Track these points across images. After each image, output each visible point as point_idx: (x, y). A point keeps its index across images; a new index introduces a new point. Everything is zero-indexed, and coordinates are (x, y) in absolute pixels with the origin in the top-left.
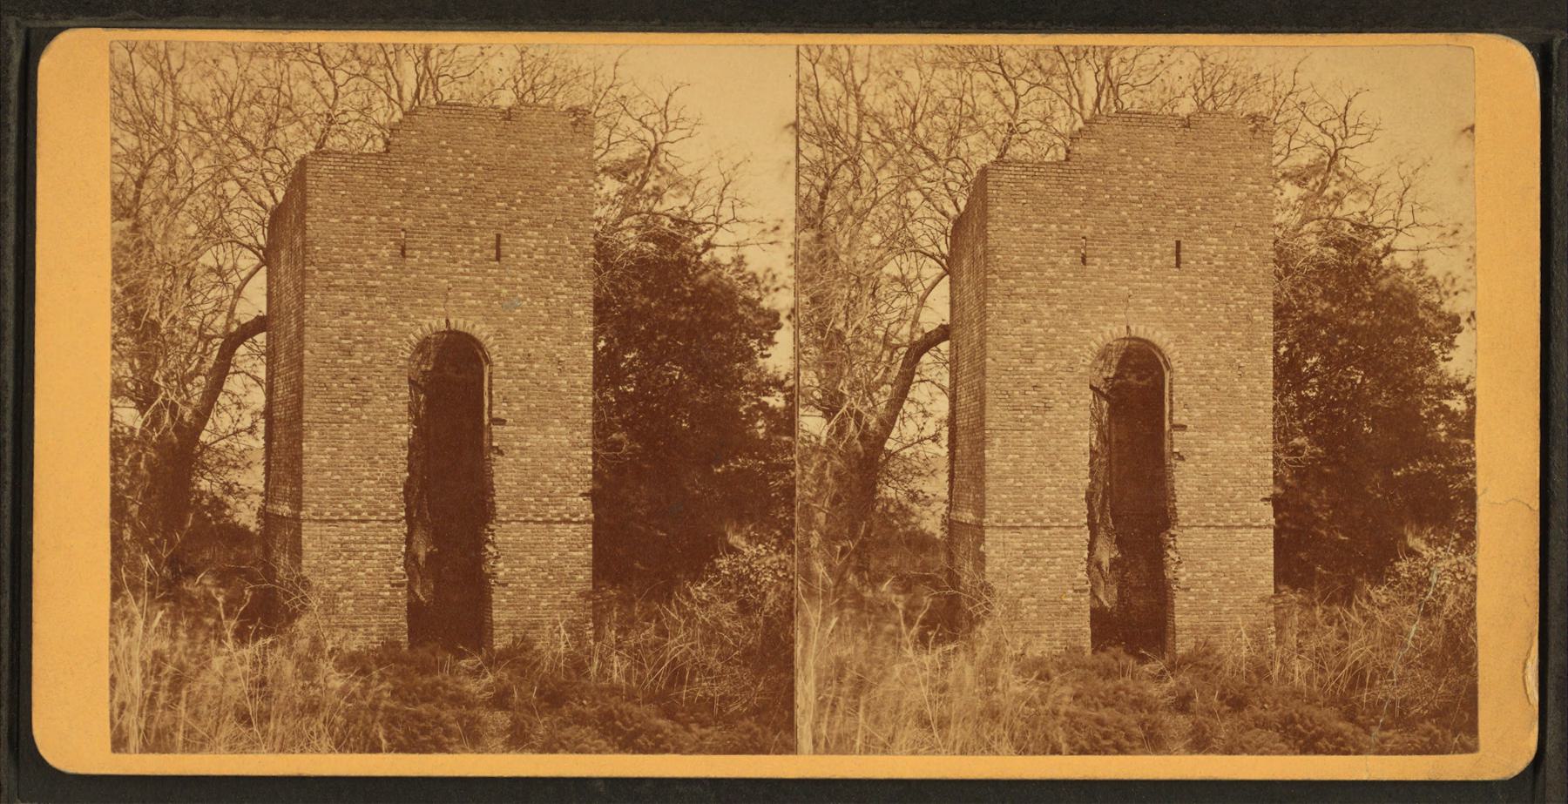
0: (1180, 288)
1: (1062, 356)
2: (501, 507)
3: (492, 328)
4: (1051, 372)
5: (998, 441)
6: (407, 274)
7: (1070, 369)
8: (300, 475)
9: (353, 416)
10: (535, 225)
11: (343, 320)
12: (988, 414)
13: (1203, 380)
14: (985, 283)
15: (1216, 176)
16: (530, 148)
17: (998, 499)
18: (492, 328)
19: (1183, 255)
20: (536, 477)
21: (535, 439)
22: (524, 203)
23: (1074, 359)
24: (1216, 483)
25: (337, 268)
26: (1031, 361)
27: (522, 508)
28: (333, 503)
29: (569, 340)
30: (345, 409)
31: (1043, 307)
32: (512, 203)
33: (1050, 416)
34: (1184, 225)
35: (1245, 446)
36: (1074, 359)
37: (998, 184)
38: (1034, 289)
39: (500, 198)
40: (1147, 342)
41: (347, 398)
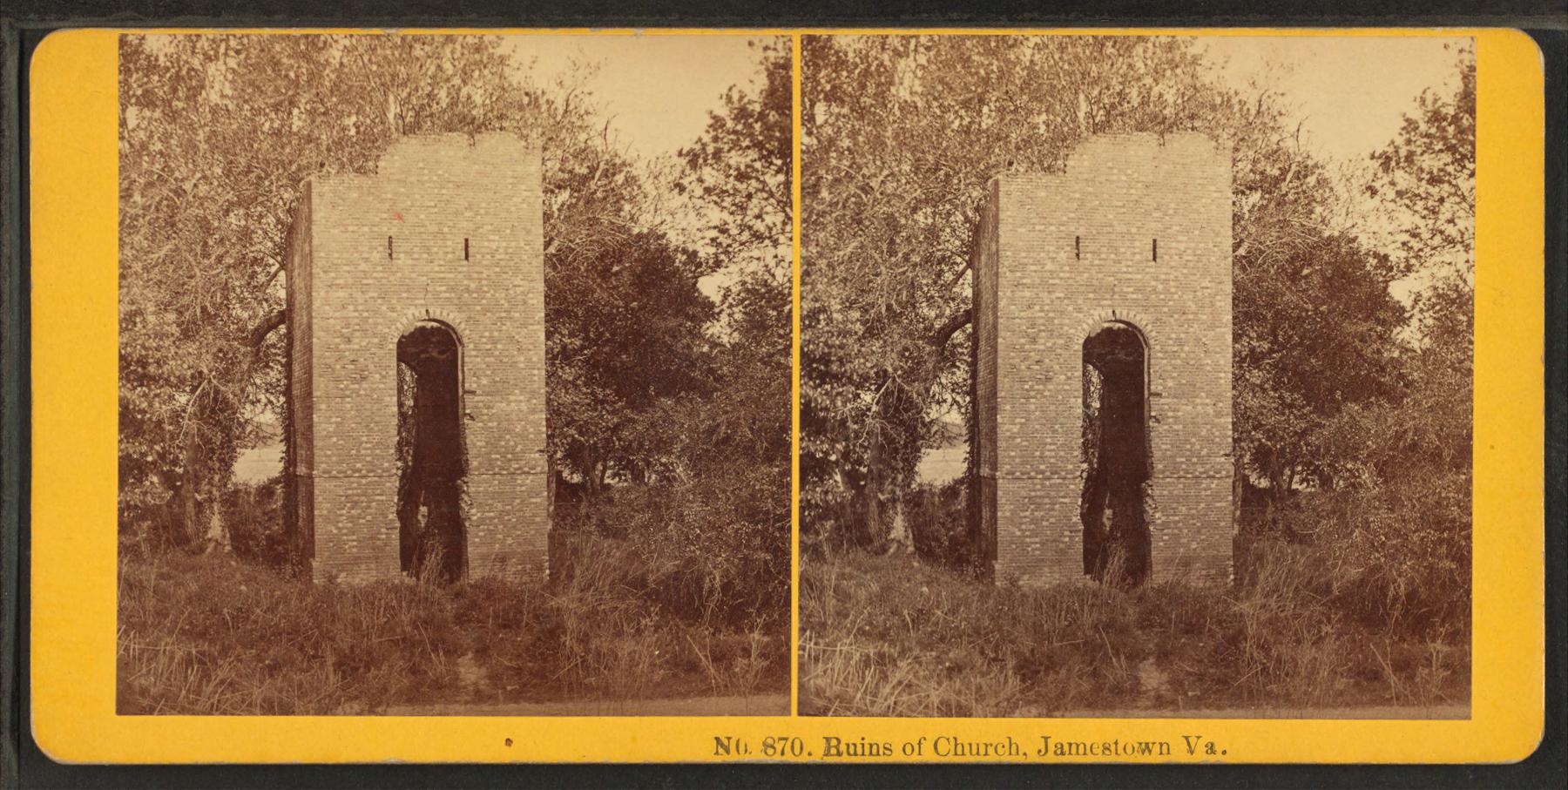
0: (1157, 279)
1: (1060, 336)
2: (474, 463)
3: (463, 315)
4: (1051, 350)
5: (323, 406)
6: (394, 273)
7: (1067, 347)
8: (311, 441)
9: (353, 391)
10: (497, 231)
11: (344, 313)
12: (315, 386)
13: (489, 353)
14: (997, 274)
15: (1186, 185)
16: (490, 168)
17: (1008, 457)
18: (463, 315)
19: (471, 250)
20: (1187, 441)
21: (1186, 409)
22: (487, 213)
23: (384, 338)
24: (501, 438)
25: (1023, 271)
26: (1034, 341)
27: (1176, 469)
28: (340, 462)
29: (1213, 327)
30: (347, 388)
31: (1044, 295)
32: (477, 214)
33: (365, 385)
34: (471, 226)
35: (524, 407)
36: (384, 338)
37: (1008, 194)
38: (351, 281)
39: (469, 208)
40: (448, 325)
41: (1032, 378)
